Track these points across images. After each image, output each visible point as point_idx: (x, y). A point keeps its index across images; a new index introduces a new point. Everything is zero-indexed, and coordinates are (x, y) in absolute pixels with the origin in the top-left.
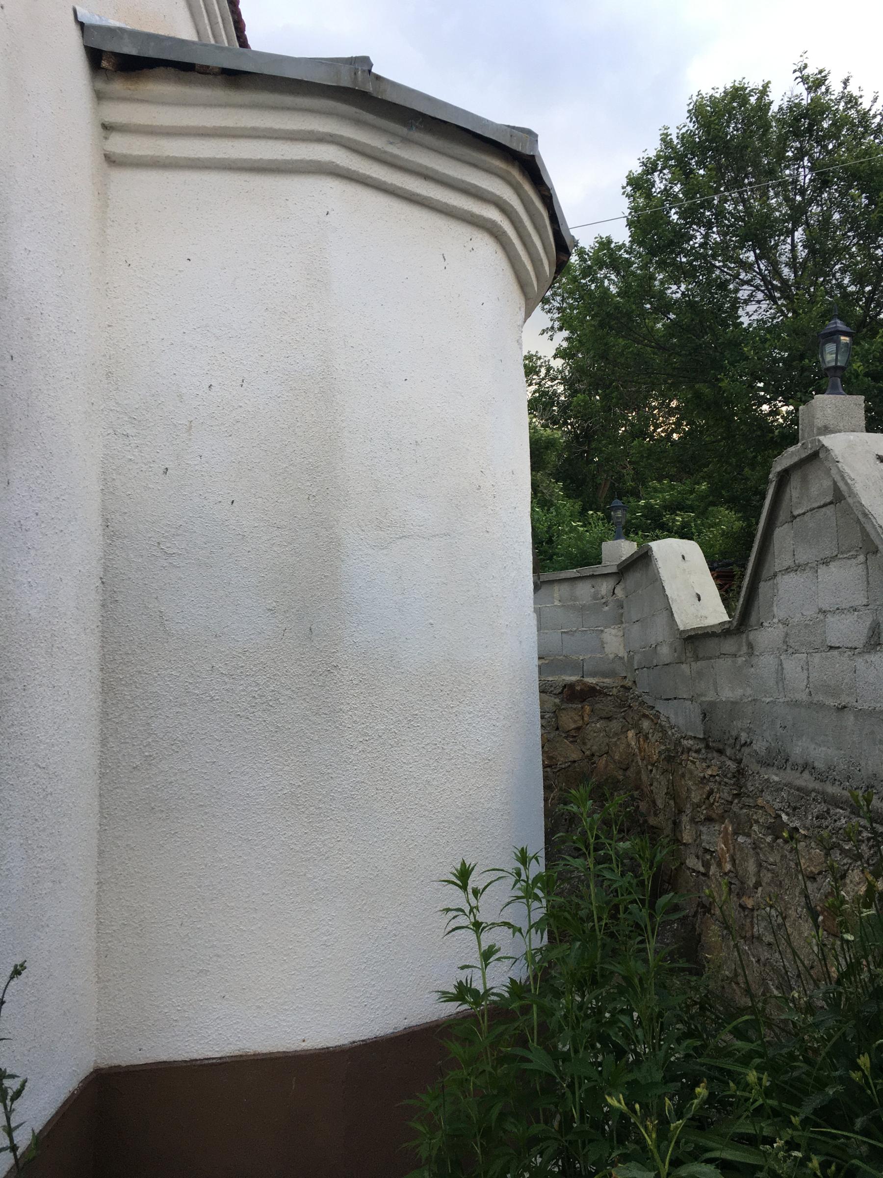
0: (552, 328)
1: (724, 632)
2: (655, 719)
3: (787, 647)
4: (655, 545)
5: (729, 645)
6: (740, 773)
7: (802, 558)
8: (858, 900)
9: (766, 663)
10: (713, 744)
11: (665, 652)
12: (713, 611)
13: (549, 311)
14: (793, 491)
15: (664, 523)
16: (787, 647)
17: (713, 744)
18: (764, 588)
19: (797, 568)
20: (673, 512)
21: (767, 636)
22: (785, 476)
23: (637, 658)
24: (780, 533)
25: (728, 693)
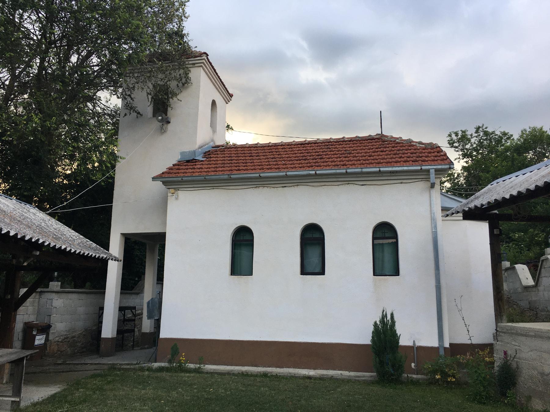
0: (459, 158)
1: (533, 287)
2: (517, 305)
3: (544, 290)
4: (516, 266)
5: (534, 289)
6: (537, 314)
7: (546, 275)
8: (83, 186)
9: (541, 293)
10: (530, 309)
11: (520, 290)
12: (530, 282)
13: (457, 151)
14: (544, 263)
15: (510, 237)
16: (544, 290)
17: (530, 309)
18: (540, 279)
19: (546, 277)
20: (514, 232)
21: (541, 288)
22: (543, 261)
23: (511, 291)
24: (543, 270)
25: (534, 299)
